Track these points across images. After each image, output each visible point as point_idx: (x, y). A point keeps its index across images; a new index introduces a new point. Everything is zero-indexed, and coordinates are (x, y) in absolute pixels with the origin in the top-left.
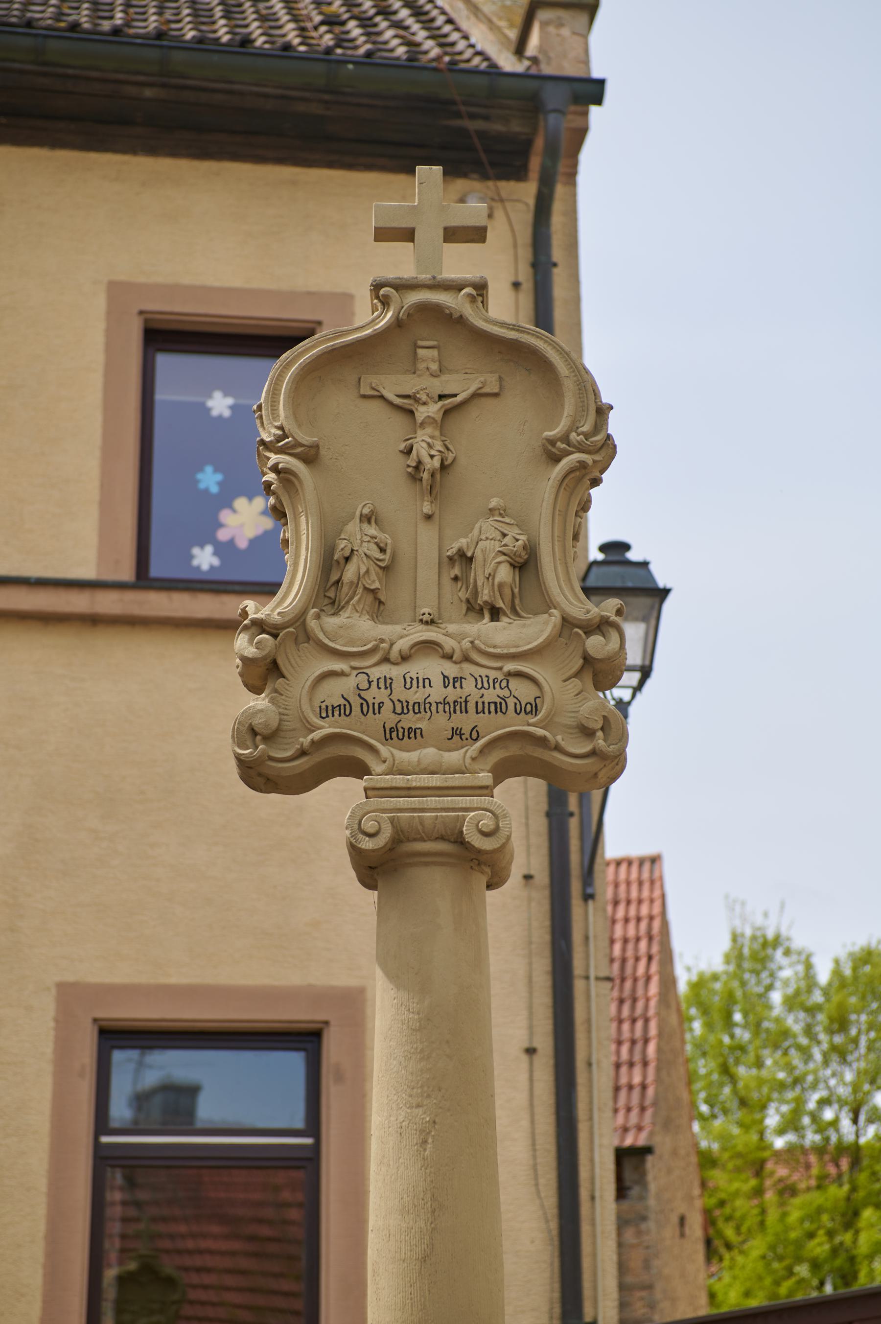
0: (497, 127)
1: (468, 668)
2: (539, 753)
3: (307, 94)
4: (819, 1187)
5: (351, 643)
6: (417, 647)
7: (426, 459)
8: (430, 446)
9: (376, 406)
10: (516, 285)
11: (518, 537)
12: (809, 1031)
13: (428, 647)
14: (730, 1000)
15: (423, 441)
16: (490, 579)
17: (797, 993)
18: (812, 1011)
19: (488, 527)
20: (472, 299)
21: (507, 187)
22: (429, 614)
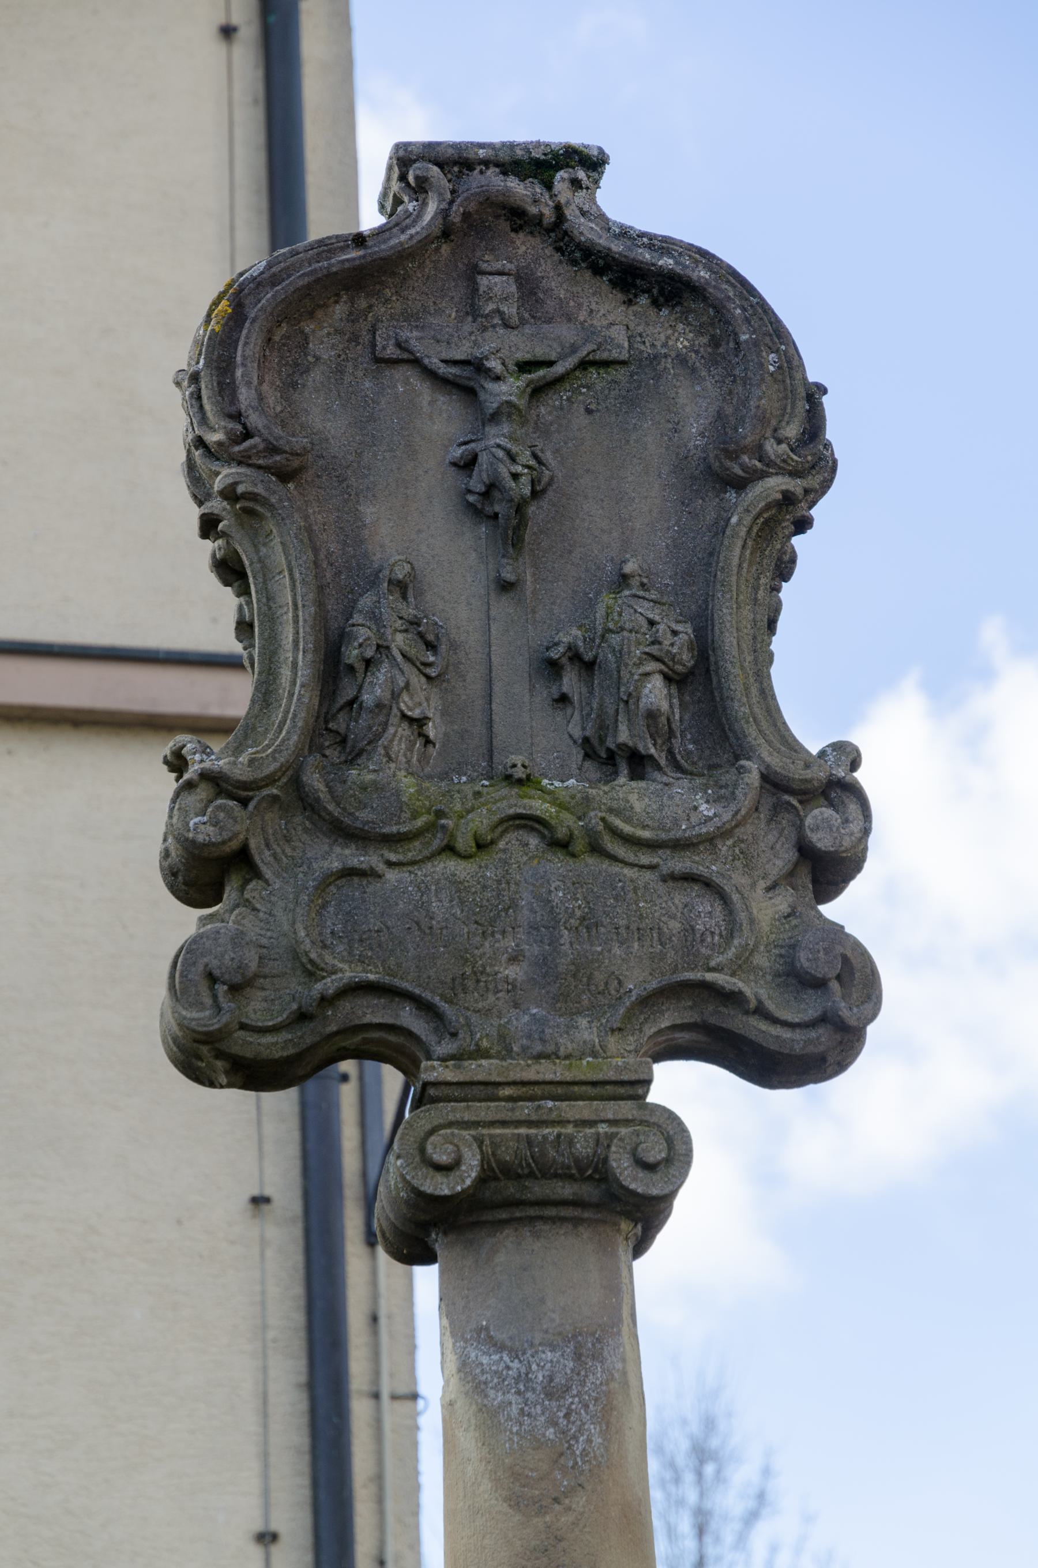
6: (505, 825)
10: (227, 32)
11: (679, 627)
15: (499, 446)
16: (631, 701)
22: (524, 766)
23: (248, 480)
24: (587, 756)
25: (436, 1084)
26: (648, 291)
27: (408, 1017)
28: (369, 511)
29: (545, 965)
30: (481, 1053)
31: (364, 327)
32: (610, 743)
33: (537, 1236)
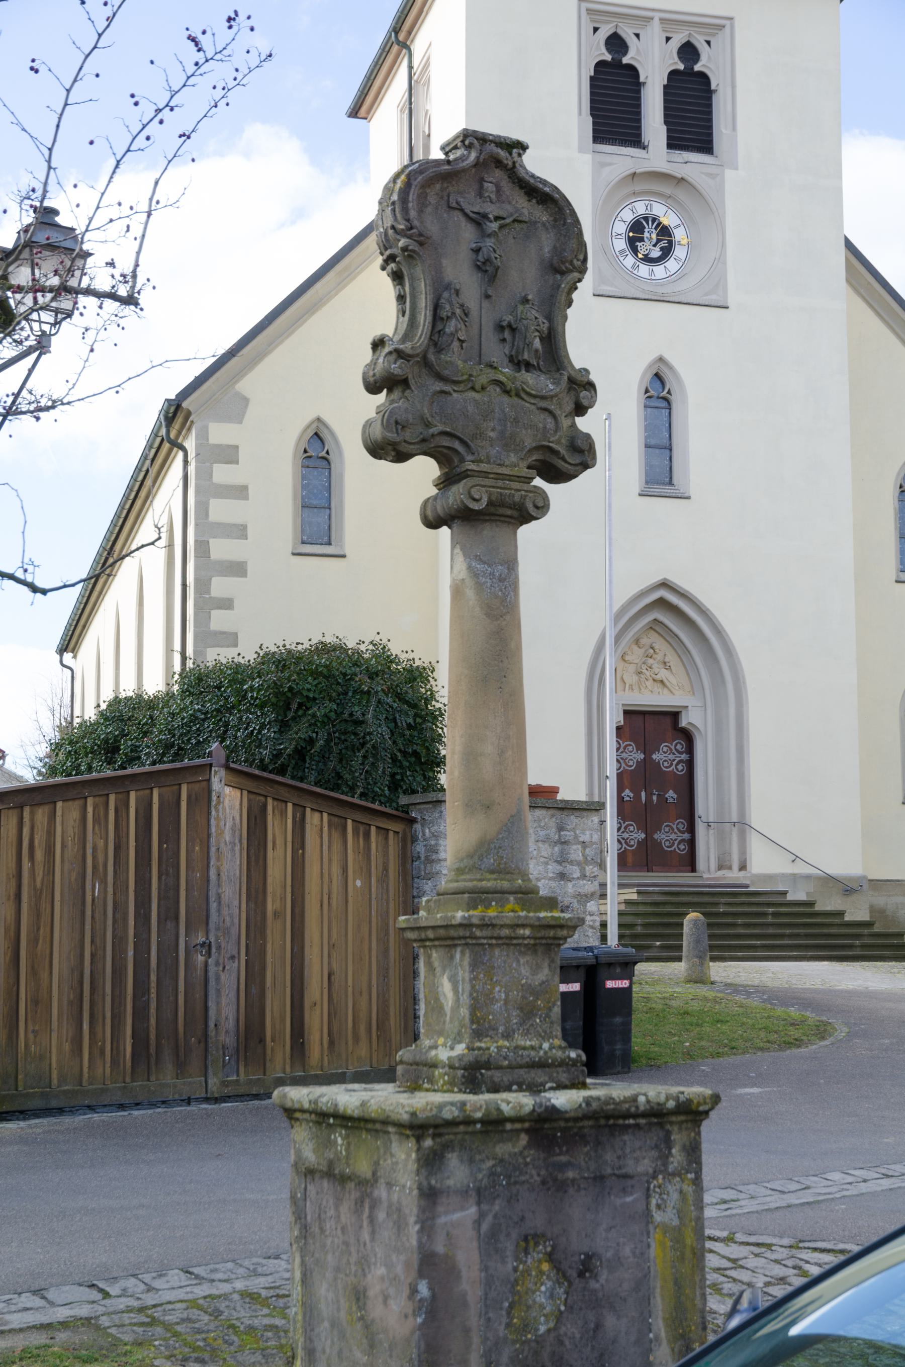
23: (413, 246)
24: (510, 361)
25: (470, 470)
26: (536, 198)
27: (457, 445)
28: (444, 262)
29: (502, 433)
30: (481, 461)
31: (445, 194)
32: (520, 358)
33: (497, 526)
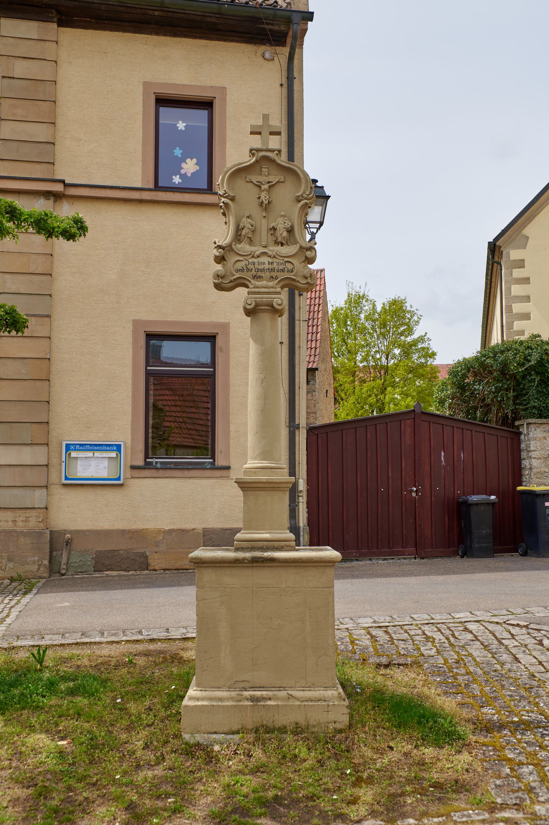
0: (276, 28)
1: (275, 260)
2: (293, 283)
3: (211, 15)
4: (373, 380)
5: (244, 252)
7: (264, 201)
8: (265, 197)
9: (250, 184)
10: (281, 85)
12: (373, 328)
13: (264, 254)
14: (347, 316)
17: (370, 315)
18: (374, 321)
19: (280, 220)
20: (277, 154)
21: (279, 49)
